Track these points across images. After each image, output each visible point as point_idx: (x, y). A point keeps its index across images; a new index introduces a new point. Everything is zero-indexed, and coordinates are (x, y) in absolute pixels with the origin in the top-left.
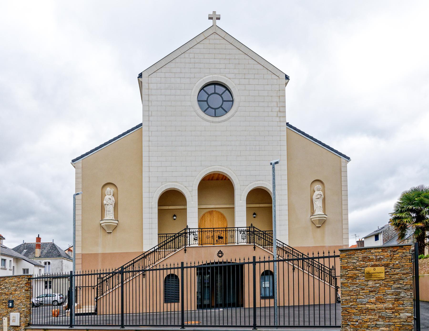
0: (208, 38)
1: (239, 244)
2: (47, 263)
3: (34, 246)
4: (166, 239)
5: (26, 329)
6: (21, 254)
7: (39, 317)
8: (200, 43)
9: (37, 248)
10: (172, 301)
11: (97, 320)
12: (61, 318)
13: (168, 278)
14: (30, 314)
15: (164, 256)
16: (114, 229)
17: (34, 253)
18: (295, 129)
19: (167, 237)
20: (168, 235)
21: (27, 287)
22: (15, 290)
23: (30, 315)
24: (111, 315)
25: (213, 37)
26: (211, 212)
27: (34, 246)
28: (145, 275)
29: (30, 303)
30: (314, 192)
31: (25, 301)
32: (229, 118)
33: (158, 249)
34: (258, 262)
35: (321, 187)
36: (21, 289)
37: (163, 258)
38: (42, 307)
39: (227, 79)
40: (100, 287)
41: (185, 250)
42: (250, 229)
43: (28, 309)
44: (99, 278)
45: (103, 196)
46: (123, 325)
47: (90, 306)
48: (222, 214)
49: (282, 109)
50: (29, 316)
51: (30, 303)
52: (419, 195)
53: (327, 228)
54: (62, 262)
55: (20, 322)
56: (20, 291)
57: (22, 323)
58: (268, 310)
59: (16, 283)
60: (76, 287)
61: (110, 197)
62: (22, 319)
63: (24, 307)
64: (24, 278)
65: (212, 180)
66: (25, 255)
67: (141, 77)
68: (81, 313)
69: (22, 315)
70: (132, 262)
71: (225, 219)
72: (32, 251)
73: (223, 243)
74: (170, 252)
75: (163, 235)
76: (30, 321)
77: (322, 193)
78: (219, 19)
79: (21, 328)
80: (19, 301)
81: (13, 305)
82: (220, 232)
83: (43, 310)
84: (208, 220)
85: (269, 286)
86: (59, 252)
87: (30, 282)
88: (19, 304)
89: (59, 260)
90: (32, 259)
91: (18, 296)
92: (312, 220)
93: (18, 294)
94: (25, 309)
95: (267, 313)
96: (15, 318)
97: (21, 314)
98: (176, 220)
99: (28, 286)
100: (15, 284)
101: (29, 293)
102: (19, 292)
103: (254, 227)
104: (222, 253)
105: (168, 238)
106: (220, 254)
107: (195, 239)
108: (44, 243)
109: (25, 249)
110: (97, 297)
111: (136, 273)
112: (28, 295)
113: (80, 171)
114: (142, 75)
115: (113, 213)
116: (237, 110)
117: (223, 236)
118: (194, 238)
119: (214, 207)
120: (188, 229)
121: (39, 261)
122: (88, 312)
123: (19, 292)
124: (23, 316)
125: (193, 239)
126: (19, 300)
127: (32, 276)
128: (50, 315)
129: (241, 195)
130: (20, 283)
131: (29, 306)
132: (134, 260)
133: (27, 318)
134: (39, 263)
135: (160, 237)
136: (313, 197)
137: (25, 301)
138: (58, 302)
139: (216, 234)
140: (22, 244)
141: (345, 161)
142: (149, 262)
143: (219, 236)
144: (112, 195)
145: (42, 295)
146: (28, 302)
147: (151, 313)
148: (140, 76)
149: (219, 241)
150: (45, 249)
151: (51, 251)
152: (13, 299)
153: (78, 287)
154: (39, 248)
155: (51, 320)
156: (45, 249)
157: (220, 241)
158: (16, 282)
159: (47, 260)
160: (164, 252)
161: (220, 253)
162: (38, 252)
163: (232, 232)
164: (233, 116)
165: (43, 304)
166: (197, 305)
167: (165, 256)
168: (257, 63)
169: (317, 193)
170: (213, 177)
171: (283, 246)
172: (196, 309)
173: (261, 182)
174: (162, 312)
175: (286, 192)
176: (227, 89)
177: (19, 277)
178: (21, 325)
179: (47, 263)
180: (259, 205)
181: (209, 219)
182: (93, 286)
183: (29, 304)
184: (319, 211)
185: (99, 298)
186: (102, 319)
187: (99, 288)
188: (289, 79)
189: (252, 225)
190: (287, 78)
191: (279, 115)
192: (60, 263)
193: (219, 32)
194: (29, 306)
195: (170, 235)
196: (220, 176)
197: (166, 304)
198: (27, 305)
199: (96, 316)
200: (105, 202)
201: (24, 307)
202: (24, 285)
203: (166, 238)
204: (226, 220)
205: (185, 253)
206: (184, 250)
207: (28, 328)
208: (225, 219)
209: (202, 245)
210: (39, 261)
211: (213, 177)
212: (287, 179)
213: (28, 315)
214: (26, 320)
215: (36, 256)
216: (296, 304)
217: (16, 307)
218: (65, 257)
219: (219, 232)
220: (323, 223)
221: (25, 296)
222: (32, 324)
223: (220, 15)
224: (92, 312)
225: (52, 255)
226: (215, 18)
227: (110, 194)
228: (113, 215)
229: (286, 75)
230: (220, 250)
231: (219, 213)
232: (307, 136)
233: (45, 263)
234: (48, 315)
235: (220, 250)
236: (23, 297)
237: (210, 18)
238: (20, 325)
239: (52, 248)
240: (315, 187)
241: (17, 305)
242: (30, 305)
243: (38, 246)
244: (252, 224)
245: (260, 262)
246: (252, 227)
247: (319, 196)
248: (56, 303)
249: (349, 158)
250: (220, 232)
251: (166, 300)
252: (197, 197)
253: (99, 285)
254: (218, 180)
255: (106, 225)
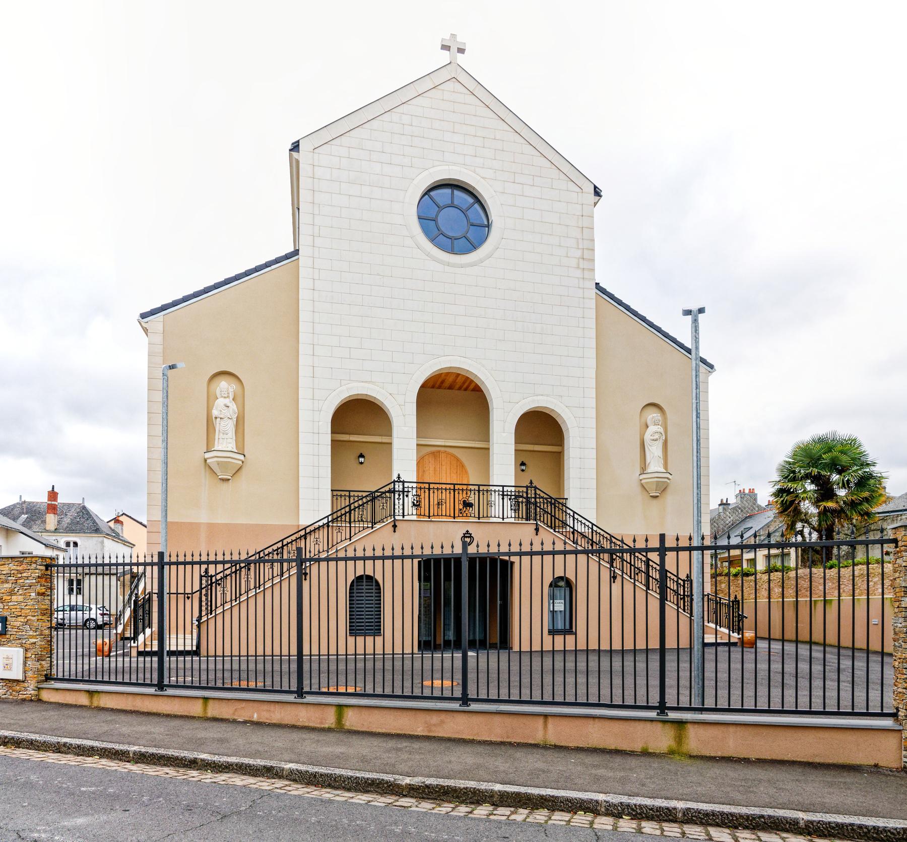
0: (439, 87)
1: (506, 520)
2: (72, 544)
3: (44, 508)
4: (347, 503)
5: (39, 688)
6: (16, 522)
7: (67, 655)
8: (424, 95)
9: (49, 511)
10: (367, 633)
11: (223, 670)
12: (120, 659)
13: (357, 582)
14: (51, 652)
15: (348, 537)
16: (237, 472)
17: (44, 522)
18: (612, 297)
19: (350, 497)
20: (352, 494)
21: (41, 585)
22: (11, 593)
23: (51, 654)
24: (252, 656)
25: (450, 85)
26: (435, 455)
27: (44, 508)
28: (307, 574)
29: (51, 624)
30: (647, 427)
31: (38, 620)
32: (482, 261)
33: (332, 521)
34: (671, 549)
35: (660, 418)
36: (26, 589)
37: (346, 539)
38: (64, 631)
39: (479, 178)
40: (206, 595)
41: (395, 526)
42: (527, 490)
43: (45, 641)
44: (206, 577)
45: (210, 400)
46: (302, 692)
47: (181, 636)
48: (458, 460)
49: (587, 255)
50: (48, 657)
51: (51, 624)
52: (830, 450)
53: (670, 499)
54: (102, 542)
55: (25, 672)
56: (25, 594)
57: (30, 674)
58: (570, 658)
59: (13, 574)
60: (149, 593)
61: (227, 401)
62: (29, 663)
63: (35, 634)
64: (35, 563)
65: (440, 387)
66: (23, 525)
67: (296, 149)
68: (153, 650)
69: (29, 655)
70: (280, 545)
71: (464, 470)
72: (38, 518)
73: (473, 515)
74: (361, 529)
75: (343, 493)
76: (51, 669)
77: (661, 430)
78: (461, 51)
79: (26, 685)
80: (23, 620)
81: (6, 628)
82: (467, 494)
83: (67, 637)
84: (431, 469)
85: (563, 609)
86: (97, 524)
87: (51, 575)
88: (21, 628)
89: (96, 539)
90: (40, 534)
91: (18, 607)
92: (642, 482)
93: (19, 603)
94: (36, 640)
95: (582, 665)
96: (10, 661)
97: (26, 650)
98: (363, 465)
99: (46, 584)
100: (9, 578)
101: (48, 602)
102: (21, 598)
103: (536, 488)
104: (470, 537)
105: (352, 501)
106: (467, 537)
107: (414, 505)
108: (64, 504)
109: (23, 513)
110: (200, 617)
111: (310, 564)
112: (46, 607)
113: (158, 339)
114: (298, 145)
115: (234, 438)
116: (499, 245)
117: (473, 502)
118: (413, 503)
119: (443, 444)
120: (401, 482)
121: (54, 538)
122: (175, 649)
123: (21, 598)
124: (33, 656)
125: (411, 505)
126: (21, 616)
127: (54, 558)
128: (90, 651)
129: (504, 422)
130: (24, 575)
131: (48, 634)
132: (282, 541)
133: (43, 663)
134: (55, 542)
135: (335, 498)
136: (645, 438)
137: (38, 620)
138: (96, 623)
139: (461, 497)
140: (18, 504)
141: (704, 371)
142: (317, 546)
143: (464, 501)
144: (231, 399)
145: (64, 606)
146: (44, 624)
147: (341, 655)
148: (296, 147)
149: (465, 512)
150: (66, 515)
151: (78, 520)
152: (6, 614)
153: (155, 593)
154: (54, 513)
155: (93, 666)
156: (66, 515)
157: (466, 512)
158: (12, 572)
159: (72, 538)
160: (348, 529)
161: (467, 537)
162: (51, 521)
163: (483, 494)
164: (489, 256)
165: (65, 625)
166: (419, 642)
167: (350, 537)
168: (540, 155)
169: (652, 429)
170: (443, 382)
171: (592, 529)
172: (416, 650)
173: (545, 398)
174: (352, 655)
175: (593, 423)
176: (477, 200)
177: (22, 559)
178: (28, 679)
179: (72, 544)
180: (532, 446)
181: (432, 469)
182: (187, 594)
183: (48, 628)
184: (655, 465)
185: (204, 619)
186: (219, 666)
187: (204, 598)
188: (600, 196)
189: (531, 482)
190: (597, 192)
191: (581, 266)
192: (99, 545)
193: (462, 78)
194: (47, 632)
195: (356, 494)
196: (457, 381)
197: (354, 637)
198: (42, 631)
199: (196, 658)
200: (215, 412)
201: (35, 634)
202: (34, 581)
203: (347, 498)
204: (466, 472)
205: (395, 531)
206: (393, 526)
207: (45, 685)
208: (464, 470)
209: (479, 518)
210: (54, 538)
211: (443, 382)
212: (595, 396)
213: (44, 655)
214: (39, 667)
215: (47, 529)
216: (617, 646)
217: (14, 633)
218: (108, 534)
219: (465, 492)
220: (664, 490)
221: (36, 607)
222: (57, 676)
223: (465, 43)
224: (186, 649)
225: (82, 529)
226: (454, 49)
227: (228, 397)
228: (234, 442)
229: (595, 187)
230: (467, 531)
231: (453, 458)
232: (635, 313)
233: (68, 544)
234: (86, 650)
235: (467, 531)
236: (32, 610)
237: (445, 47)
238: (25, 677)
239: (81, 514)
240: (649, 417)
241: (16, 630)
242: (51, 630)
243: (52, 509)
244: (531, 481)
245: (677, 549)
246: (399, 482)
247: (657, 436)
248: (93, 625)
249: (711, 367)
250: (467, 494)
251: (355, 629)
252: (415, 417)
253: (204, 591)
254: (452, 389)
255: (218, 463)
